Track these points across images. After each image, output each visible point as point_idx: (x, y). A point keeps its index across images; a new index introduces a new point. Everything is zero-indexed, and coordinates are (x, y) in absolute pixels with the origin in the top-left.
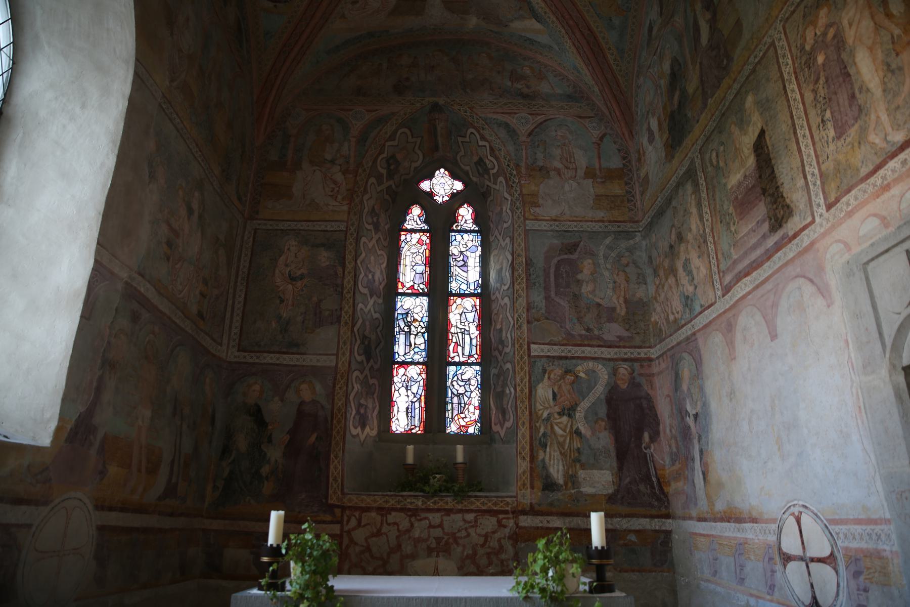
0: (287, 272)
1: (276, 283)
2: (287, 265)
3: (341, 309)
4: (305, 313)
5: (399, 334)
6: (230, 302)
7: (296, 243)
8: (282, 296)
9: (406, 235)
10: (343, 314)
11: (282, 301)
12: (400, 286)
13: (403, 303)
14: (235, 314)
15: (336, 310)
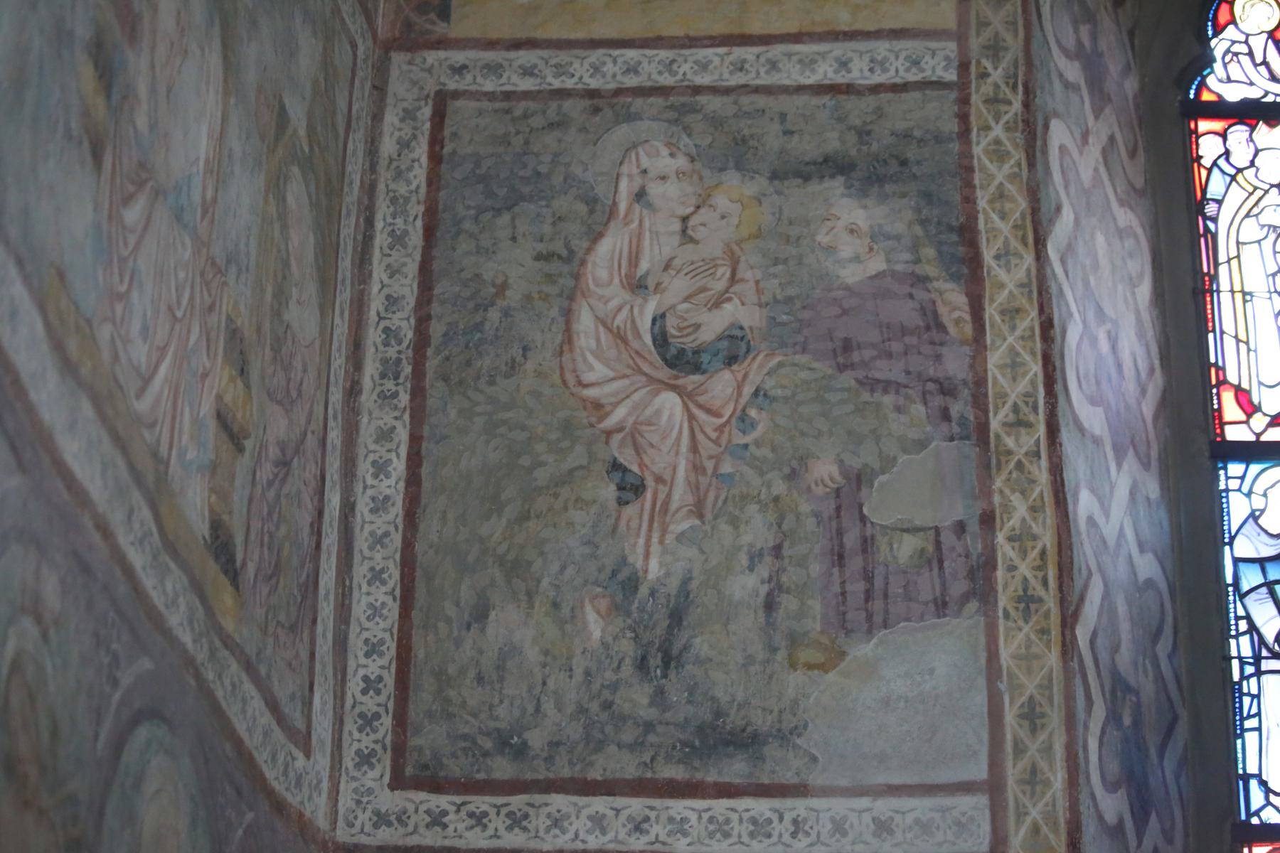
0: (645, 324)
1: (581, 384)
2: (638, 286)
3: (988, 520)
4: (777, 550)
5: (1259, 673)
6: (334, 500)
7: (681, 162)
8: (627, 458)
9: (1223, 135)
10: (1005, 550)
11: (631, 488)
12: (1231, 410)
13: (1258, 503)
14: (360, 571)
15: (960, 528)
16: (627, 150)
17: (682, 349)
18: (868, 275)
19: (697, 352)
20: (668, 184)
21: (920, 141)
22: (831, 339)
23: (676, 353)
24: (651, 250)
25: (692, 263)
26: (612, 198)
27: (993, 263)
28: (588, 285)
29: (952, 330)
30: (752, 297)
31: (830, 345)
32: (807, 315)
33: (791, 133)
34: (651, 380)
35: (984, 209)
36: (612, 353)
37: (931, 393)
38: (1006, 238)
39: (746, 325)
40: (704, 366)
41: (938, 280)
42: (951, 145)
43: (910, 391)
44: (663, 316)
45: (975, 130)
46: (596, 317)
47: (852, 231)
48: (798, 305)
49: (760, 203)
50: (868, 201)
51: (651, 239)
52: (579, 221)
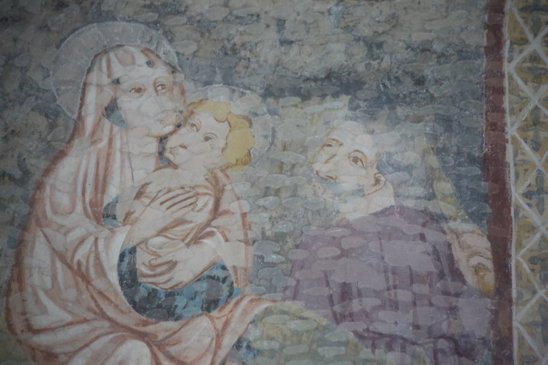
16: (96, 56)
17: (154, 290)
18: (372, 211)
19: (171, 295)
20: (144, 97)
21: (441, 56)
22: (328, 285)
23: (146, 295)
24: (122, 172)
25: (169, 191)
26: (77, 113)
27: (522, 202)
28: (44, 212)
29: (470, 278)
30: (237, 232)
31: (326, 291)
32: (299, 255)
33: (291, 43)
34: (115, 325)
35: (514, 138)
36: (71, 294)
37: (443, 352)
38: (539, 172)
39: (229, 264)
40: (178, 311)
41: (455, 220)
42: (478, 62)
43: (418, 349)
44: (133, 251)
45: (508, 43)
46: (53, 249)
47: (356, 160)
48: (290, 243)
49: (251, 124)
50: (374, 126)
51: (122, 161)
52: (36, 136)
